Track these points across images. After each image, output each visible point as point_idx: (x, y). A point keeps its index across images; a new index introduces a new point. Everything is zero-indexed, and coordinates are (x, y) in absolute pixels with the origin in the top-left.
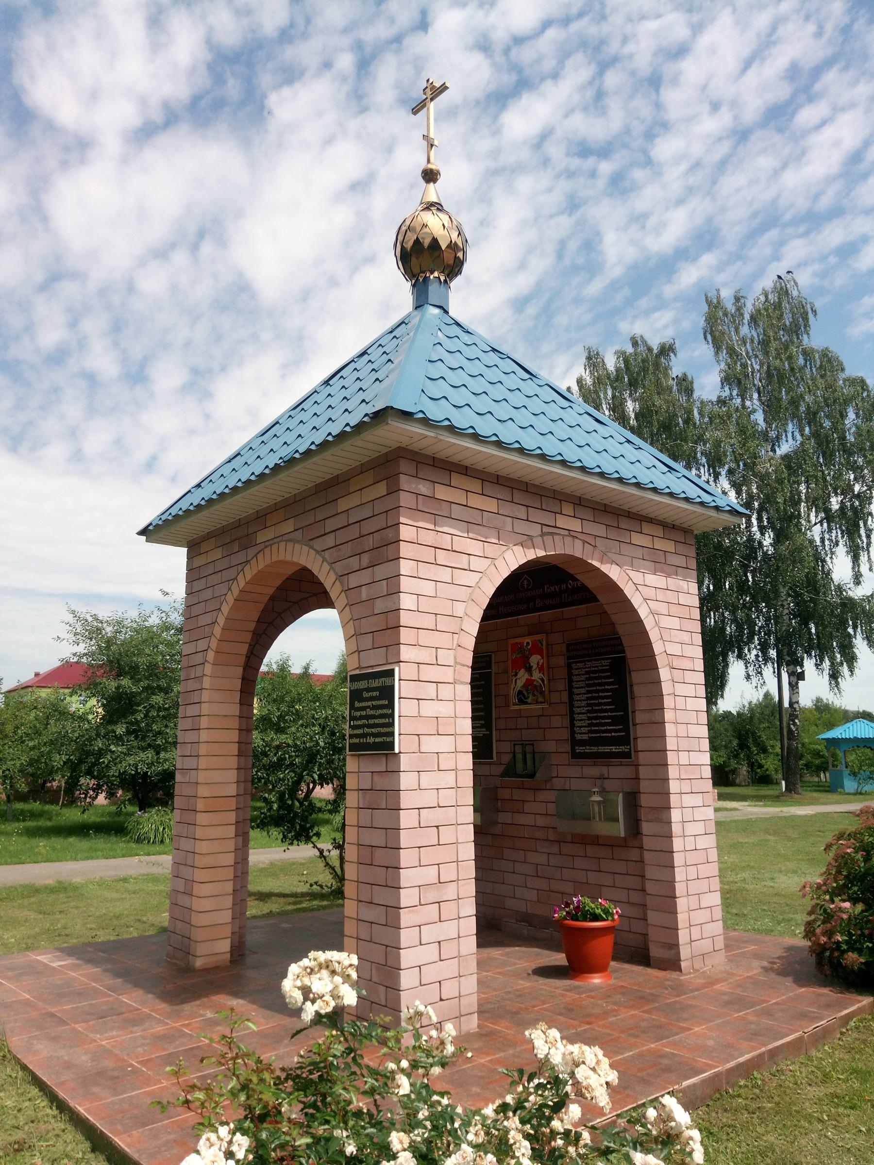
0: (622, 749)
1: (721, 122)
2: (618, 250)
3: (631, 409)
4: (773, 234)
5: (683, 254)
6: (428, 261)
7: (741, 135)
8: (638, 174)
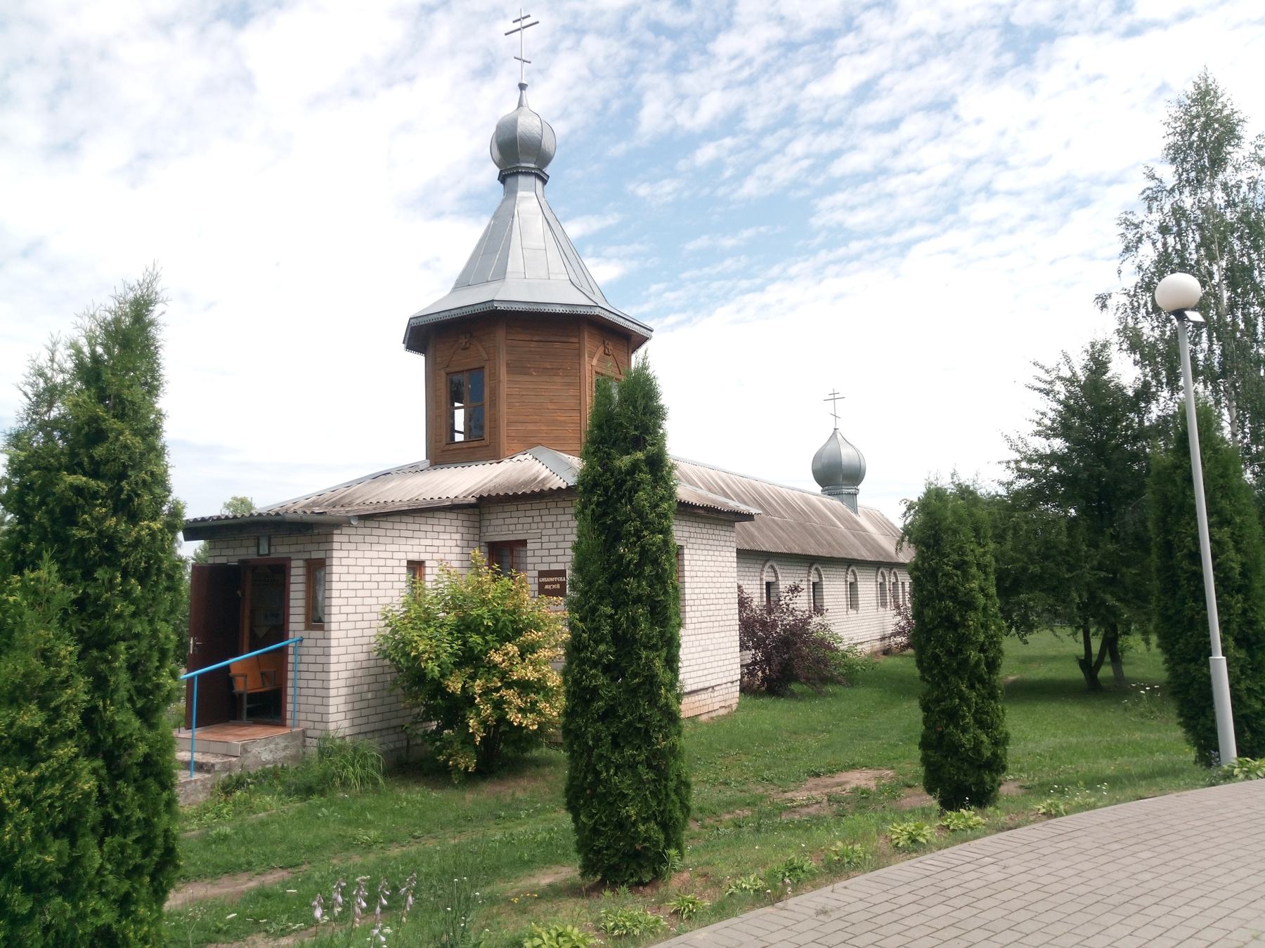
0: (544, 580)
1: (777, 33)
2: (652, 115)
3: (1154, 556)
4: (785, 132)
5: (709, 135)
6: (978, 121)
7: (790, 47)
8: (695, 59)
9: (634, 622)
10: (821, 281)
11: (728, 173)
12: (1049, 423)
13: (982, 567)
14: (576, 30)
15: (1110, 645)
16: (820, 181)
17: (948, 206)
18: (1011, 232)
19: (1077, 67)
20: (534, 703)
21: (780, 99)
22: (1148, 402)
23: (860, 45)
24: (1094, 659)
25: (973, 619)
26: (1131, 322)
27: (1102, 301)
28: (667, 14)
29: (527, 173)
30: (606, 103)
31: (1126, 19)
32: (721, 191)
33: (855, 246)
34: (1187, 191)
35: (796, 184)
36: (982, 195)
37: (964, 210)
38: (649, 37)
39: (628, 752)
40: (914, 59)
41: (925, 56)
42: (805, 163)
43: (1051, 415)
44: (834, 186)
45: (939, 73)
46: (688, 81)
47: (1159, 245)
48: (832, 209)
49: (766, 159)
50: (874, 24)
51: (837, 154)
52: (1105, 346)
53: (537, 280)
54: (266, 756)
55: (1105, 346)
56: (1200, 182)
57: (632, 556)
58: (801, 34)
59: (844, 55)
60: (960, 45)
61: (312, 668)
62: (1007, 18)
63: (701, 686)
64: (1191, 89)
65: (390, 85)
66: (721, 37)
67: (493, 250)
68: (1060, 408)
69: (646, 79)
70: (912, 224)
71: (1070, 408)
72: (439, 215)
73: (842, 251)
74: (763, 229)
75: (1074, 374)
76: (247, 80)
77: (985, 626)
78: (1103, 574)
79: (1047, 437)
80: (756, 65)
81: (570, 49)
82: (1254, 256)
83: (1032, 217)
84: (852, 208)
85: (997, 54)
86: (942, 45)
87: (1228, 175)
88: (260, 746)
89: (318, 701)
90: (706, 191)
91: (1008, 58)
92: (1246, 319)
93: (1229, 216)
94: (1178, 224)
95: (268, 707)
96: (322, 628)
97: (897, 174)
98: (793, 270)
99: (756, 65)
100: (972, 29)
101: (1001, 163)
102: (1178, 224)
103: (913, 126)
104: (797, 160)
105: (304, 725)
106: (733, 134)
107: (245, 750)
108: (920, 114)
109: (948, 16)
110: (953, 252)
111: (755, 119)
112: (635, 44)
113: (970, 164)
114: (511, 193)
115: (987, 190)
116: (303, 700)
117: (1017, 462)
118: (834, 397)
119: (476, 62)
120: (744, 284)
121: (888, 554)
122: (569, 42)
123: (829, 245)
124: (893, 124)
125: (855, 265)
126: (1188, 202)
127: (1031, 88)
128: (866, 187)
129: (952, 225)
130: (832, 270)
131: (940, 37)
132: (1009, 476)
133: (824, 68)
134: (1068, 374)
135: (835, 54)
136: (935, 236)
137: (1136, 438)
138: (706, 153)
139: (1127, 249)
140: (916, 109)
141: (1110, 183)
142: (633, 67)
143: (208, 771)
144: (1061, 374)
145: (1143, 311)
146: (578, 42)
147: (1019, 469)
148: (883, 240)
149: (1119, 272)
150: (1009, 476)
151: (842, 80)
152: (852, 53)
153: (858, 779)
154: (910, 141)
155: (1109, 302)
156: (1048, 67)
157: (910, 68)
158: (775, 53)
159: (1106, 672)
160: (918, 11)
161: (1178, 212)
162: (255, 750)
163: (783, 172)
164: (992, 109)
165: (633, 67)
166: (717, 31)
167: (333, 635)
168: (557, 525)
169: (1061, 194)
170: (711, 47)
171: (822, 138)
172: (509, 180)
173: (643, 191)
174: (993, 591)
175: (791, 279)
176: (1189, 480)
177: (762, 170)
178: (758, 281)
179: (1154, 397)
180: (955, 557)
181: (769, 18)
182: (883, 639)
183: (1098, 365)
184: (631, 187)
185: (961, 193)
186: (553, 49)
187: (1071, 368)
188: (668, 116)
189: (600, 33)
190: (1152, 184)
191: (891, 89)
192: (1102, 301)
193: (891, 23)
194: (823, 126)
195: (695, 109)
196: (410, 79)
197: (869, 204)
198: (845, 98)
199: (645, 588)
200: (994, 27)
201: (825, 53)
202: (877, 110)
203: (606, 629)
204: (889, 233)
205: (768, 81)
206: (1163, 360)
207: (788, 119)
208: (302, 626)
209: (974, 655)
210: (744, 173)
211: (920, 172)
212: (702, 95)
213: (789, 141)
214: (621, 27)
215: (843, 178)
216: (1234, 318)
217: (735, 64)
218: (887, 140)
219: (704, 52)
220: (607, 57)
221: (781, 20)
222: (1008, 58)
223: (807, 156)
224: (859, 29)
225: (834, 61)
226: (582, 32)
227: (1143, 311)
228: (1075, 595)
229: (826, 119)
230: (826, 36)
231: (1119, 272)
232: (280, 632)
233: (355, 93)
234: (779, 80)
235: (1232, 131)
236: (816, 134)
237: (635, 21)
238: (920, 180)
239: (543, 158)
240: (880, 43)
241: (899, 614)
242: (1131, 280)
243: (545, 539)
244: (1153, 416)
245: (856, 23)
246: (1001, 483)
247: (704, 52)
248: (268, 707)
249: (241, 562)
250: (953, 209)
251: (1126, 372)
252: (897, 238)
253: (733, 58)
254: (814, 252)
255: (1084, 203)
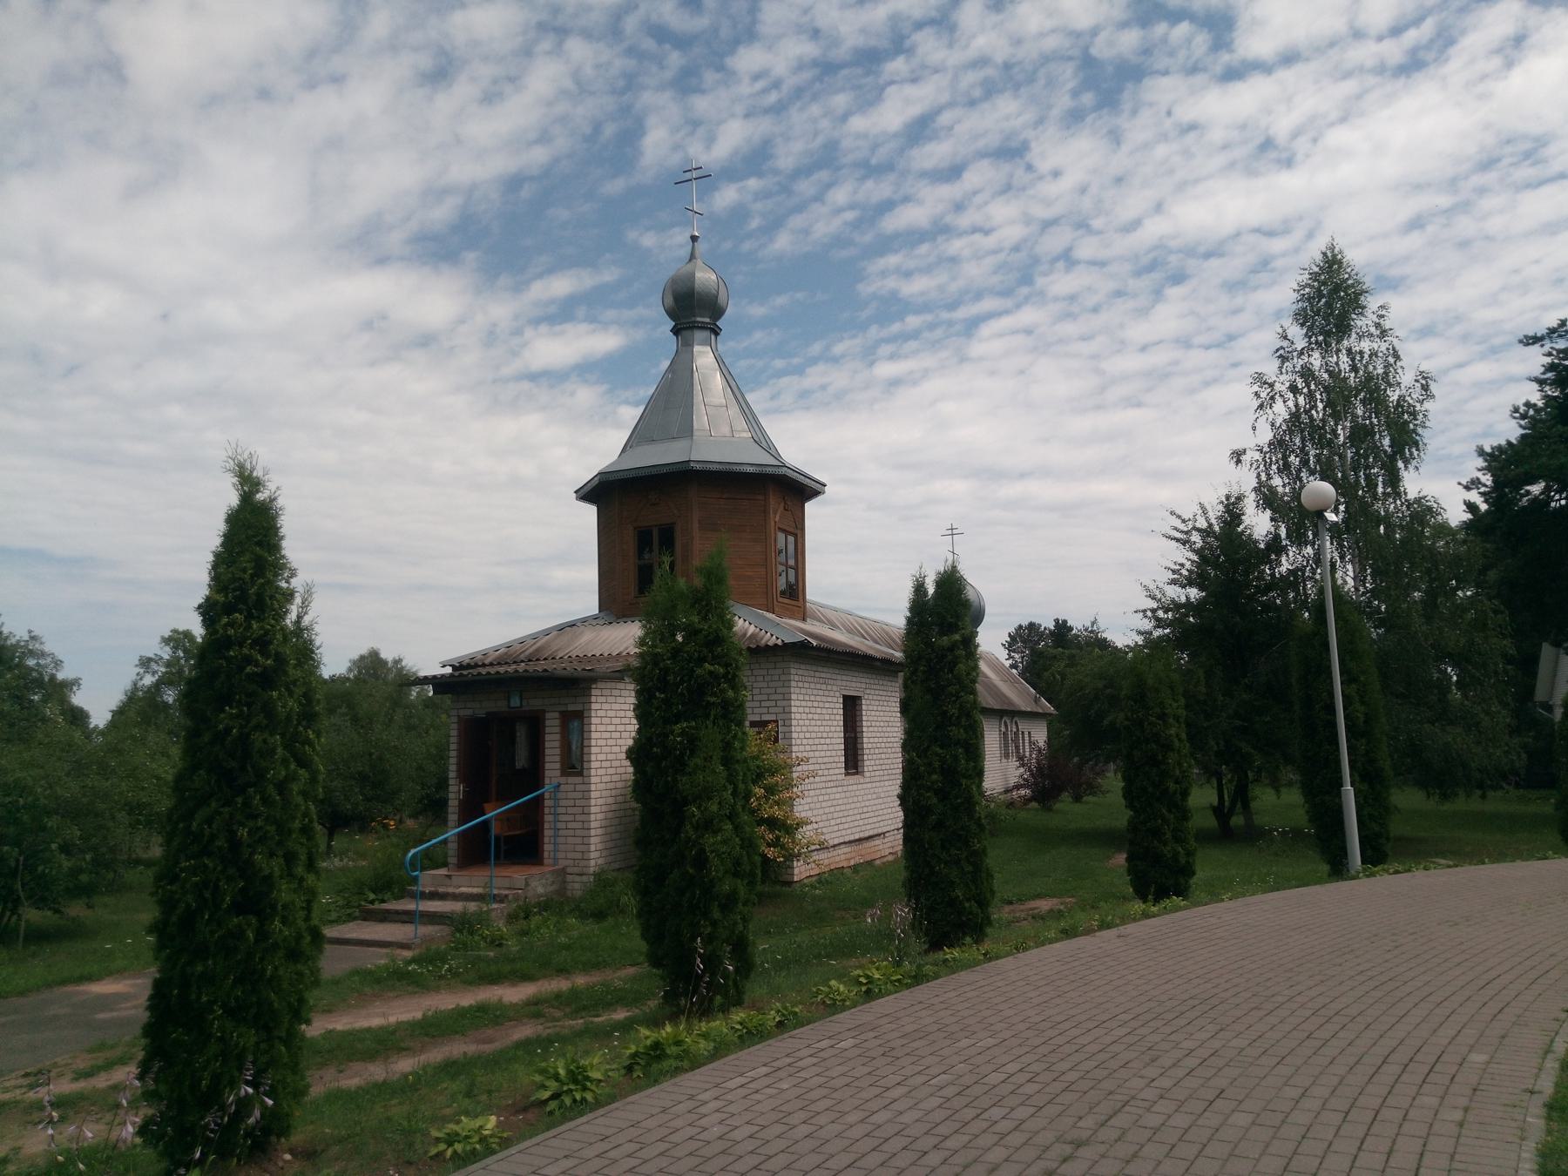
1: (807, 49)
2: (658, 145)
4: (824, 175)
5: (733, 172)
7: (826, 69)
8: (710, 77)
9: (955, 758)
10: (872, 364)
11: (755, 223)
12: (1185, 572)
13: (1177, 718)
14: (553, 29)
15: (1242, 795)
16: (868, 238)
17: (1021, 276)
18: (1095, 310)
19: (1169, 113)
20: (778, 838)
21: (816, 134)
22: (1279, 555)
23: (913, 71)
24: (1239, 805)
25: (1172, 759)
26: (1264, 477)
27: (1238, 456)
28: (670, 14)
29: (703, 327)
30: (597, 127)
31: (1225, 58)
32: (747, 246)
33: (913, 321)
34: (1316, 355)
35: (839, 241)
36: (1061, 265)
37: (1040, 282)
38: (649, 44)
39: (954, 851)
40: (977, 93)
41: (990, 90)
42: (850, 216)
43: (1188, 565)
44: (886, 245)
45: (1006, 113)
46: (702, 104)
47: (1291, 404)
48: (884, 274)
49: (800, 208)
50: (929, 46)
51: (887, 206)
52: (1240, 498)
53: (716, 437)
54: (540, 890)
55: (1240, 498)
56: (1328, 345)
57: (954, 711)
58: (841, 53)
59: (892, 83)
60: (1031, 79)
61: (570, 810)
62: (1086, 49)
63: (867, 834)
64: (1319, 258)
65: (311, 85)
66: (742, 51)
67: (671, 404)
68: (1195, 558)
69: (647, 98)
70: (978, 296)
71: (1205, 558)
72: (382, 261)
73: (896, 327)
74: (799, 295)
75: (1210, 525)
76: (113, 69)
77: (1180, 764)
78: (1238, 723)
79: (1183, 587)
80: (785, 88)
81: (549, 53)
82: (1375, 421)
83: (1119, 294)
84: (908, 274)
85: (1075, 93)
86: (1009, 77)
87: (1350, 342)
88: (532, 882)
89: (579, 840)
90: (727, 245)
91: (1088, 98)
92: (1367, 477)
93: (1352, 380)
94: (1308, 386)
95: (524, 845)
96: (580, 774)
97: (960, 235)
98: (839, 349)
99: (785, 88)
100: (1046, 59)
101: (1083, 225)
102: (1308, 386)
103: (979, 176)
104: (839, 211)
105: (562, 863)
106: (759, 174)
107: (527, 884)
108: (985, 162)
109: (1018, 42)
110: (1028, 331)
111: (787, 158)
112: (631, 51)
113: (1047, 225)
114: (685, 347)
115: (1067, 259)
116: (562, 840)
117: (1154, 611)
118: (952, 531)
119: (425, 62)
120: (779, 363)
121: (1011, 703)
122: (546, 45)
123: (883, 318)
124: (953, 172)
125: (913, 345)
126: (1316, 360)
127: (1115, 137)
128: (924, 248)
129: (1027, 299)
130: (885, 349)
131: (1007, 66)
132: (1147, 625)
133: (870, 99)
134: (1204, 525)
135: (881, 81)
136: (1007, 312)
137: (1269, 587)
138: (727, 196)
139: (1261, 407)
140: (982, 155)
141: (1208, 255)
142: (630, 83)
143: (501, 901)
144: (1198, 525)
145: (1274, 467)
146: (560, 44)
147: (1158, 619)
148: (945, 315)
149: (1254, 429)
150: (1147, 625)
151: (892, 114)
152: (902, 82)
153: (1044, 905)
154: (975, 193)
155: (1243, 458)
156: (1135, 112)
157: (972, 103)
158: (807, 75)
159: (1237, 820)
160: (982, 35)
161: (1307, 373)
162: (533, 884)
163: (823, 224)
164: (1071, 159)
165: (630, 83)
166: (735, 43)
167: (593, 780)
168: (768, 678)
169: (1152, 267)
170: (730, 62)
171: (870, 184)
172: (686, 333)
173: (648, 240)
174: (1184, 736)
175: (835, 360)
176: (1326, 646)
177: (797, 221)
178: (796, 361)
179: (1284, 550)
180: (1157, 710)
181: (800, 29)
182: (1007, 791)
183: (1232, 511)
184: (632, 235)
185: (1035, 261)
186: (527, 52)
187: (1207, 520)
188: (677, 147)
189: (587, 34)
190: (1285, 344)
191: (951, 128)
192: (1238, 456)
193: (950, 46)
194: (869, 170)
195: (710, 140)
196: (338, 80)
197: (928, 270)
198: (895, 135)
199: (962, 734)
200: (1070, 58)
201: (870, 79)
202: (935, 153)
203: (937, 764)
204: (953, 306)
205: (802, 109)
206: (1298, 519)
207: (826, 159)
208: (558, 773)
209: (1172, 786)
210: (774, 225)
211: (987, 232)
212: (720, 122)
213: (829, 186)
214: (613, 30)
215: (896, 235)
216: (1357, 477)
217: (759, 85)
218: (947, 192)
219: (721, 68)
220: (597, 66)
221: (815, 34)
222: (1088, 98)
223: (852, 207)
224: (910, 52)
225: (882, 89)
226: (562, 32)
227: (1274, 467)
228: (1212, 743)
229: (874, 161)
230: (870, 58)
231: (1254, 429)
232: (533, 776)
233: (265, 94)
234: (815, 109)
235: (1356, 299)
236: (864, 178)
237: (631, 23)
238: (989, 242)
239: (716, 311)
240: (936, 71)
241: (1023, 765)
242: (1265, 435)
243: (756, 691)
244: (1283, 569)
245: (907, 44)
246: (1140, 633)
247: (721, 68)
248: (524, 845)
249: (488, 714)
250: (1027, 279)
251: (1259, 523)
252: (962, 313)
253: (756, 77)
254: (863, 327)
255: (1178, 278)
